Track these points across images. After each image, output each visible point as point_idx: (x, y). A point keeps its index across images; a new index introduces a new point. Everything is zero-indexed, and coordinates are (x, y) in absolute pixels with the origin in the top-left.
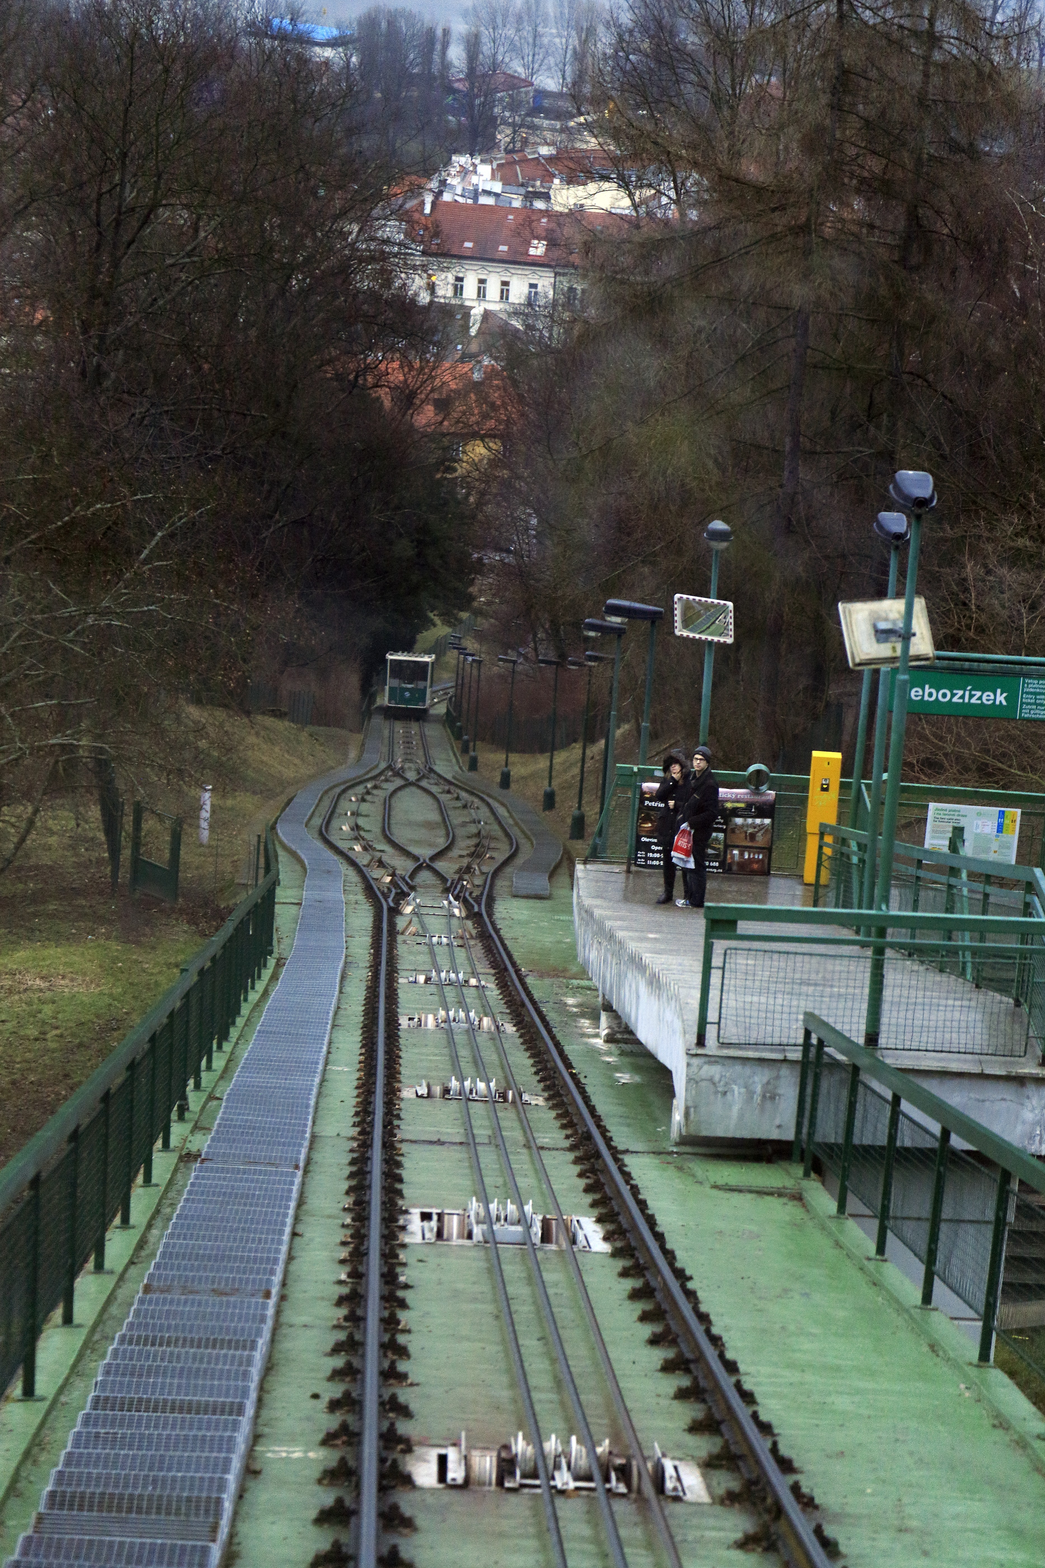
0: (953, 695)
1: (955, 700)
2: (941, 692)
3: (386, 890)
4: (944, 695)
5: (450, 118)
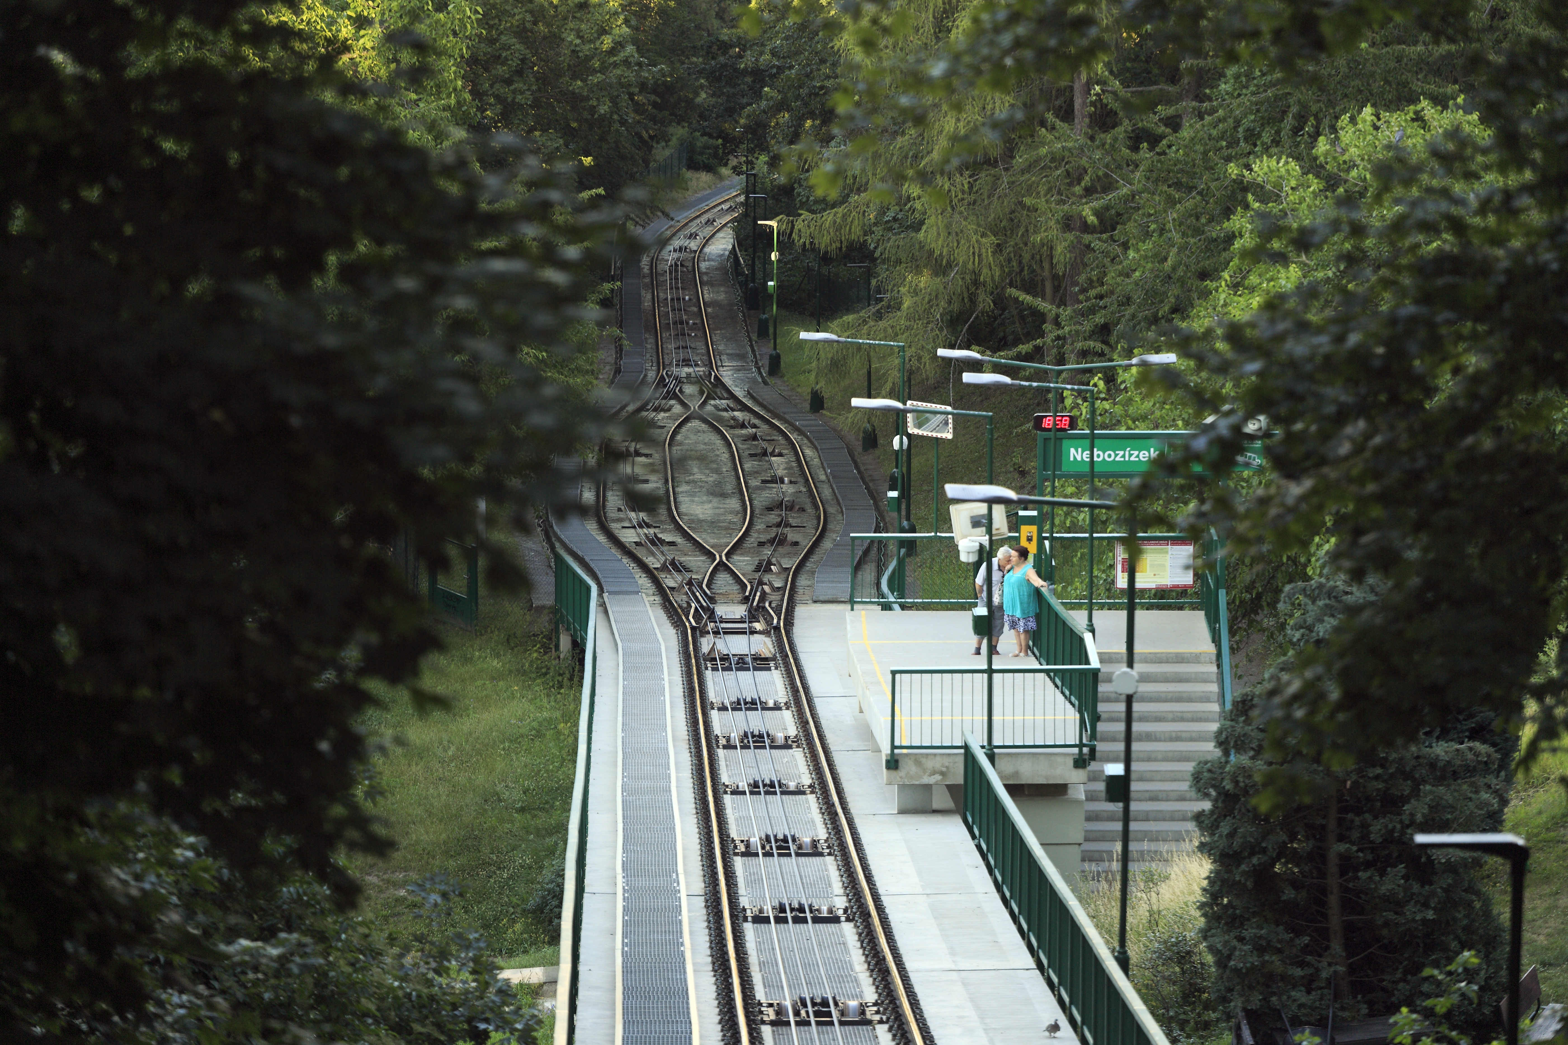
0: (1116, 455)
1: (1118, 459)
2: (1101, 459)
3: (685, 605)
4: (1110, 456)
5: (58, 57)
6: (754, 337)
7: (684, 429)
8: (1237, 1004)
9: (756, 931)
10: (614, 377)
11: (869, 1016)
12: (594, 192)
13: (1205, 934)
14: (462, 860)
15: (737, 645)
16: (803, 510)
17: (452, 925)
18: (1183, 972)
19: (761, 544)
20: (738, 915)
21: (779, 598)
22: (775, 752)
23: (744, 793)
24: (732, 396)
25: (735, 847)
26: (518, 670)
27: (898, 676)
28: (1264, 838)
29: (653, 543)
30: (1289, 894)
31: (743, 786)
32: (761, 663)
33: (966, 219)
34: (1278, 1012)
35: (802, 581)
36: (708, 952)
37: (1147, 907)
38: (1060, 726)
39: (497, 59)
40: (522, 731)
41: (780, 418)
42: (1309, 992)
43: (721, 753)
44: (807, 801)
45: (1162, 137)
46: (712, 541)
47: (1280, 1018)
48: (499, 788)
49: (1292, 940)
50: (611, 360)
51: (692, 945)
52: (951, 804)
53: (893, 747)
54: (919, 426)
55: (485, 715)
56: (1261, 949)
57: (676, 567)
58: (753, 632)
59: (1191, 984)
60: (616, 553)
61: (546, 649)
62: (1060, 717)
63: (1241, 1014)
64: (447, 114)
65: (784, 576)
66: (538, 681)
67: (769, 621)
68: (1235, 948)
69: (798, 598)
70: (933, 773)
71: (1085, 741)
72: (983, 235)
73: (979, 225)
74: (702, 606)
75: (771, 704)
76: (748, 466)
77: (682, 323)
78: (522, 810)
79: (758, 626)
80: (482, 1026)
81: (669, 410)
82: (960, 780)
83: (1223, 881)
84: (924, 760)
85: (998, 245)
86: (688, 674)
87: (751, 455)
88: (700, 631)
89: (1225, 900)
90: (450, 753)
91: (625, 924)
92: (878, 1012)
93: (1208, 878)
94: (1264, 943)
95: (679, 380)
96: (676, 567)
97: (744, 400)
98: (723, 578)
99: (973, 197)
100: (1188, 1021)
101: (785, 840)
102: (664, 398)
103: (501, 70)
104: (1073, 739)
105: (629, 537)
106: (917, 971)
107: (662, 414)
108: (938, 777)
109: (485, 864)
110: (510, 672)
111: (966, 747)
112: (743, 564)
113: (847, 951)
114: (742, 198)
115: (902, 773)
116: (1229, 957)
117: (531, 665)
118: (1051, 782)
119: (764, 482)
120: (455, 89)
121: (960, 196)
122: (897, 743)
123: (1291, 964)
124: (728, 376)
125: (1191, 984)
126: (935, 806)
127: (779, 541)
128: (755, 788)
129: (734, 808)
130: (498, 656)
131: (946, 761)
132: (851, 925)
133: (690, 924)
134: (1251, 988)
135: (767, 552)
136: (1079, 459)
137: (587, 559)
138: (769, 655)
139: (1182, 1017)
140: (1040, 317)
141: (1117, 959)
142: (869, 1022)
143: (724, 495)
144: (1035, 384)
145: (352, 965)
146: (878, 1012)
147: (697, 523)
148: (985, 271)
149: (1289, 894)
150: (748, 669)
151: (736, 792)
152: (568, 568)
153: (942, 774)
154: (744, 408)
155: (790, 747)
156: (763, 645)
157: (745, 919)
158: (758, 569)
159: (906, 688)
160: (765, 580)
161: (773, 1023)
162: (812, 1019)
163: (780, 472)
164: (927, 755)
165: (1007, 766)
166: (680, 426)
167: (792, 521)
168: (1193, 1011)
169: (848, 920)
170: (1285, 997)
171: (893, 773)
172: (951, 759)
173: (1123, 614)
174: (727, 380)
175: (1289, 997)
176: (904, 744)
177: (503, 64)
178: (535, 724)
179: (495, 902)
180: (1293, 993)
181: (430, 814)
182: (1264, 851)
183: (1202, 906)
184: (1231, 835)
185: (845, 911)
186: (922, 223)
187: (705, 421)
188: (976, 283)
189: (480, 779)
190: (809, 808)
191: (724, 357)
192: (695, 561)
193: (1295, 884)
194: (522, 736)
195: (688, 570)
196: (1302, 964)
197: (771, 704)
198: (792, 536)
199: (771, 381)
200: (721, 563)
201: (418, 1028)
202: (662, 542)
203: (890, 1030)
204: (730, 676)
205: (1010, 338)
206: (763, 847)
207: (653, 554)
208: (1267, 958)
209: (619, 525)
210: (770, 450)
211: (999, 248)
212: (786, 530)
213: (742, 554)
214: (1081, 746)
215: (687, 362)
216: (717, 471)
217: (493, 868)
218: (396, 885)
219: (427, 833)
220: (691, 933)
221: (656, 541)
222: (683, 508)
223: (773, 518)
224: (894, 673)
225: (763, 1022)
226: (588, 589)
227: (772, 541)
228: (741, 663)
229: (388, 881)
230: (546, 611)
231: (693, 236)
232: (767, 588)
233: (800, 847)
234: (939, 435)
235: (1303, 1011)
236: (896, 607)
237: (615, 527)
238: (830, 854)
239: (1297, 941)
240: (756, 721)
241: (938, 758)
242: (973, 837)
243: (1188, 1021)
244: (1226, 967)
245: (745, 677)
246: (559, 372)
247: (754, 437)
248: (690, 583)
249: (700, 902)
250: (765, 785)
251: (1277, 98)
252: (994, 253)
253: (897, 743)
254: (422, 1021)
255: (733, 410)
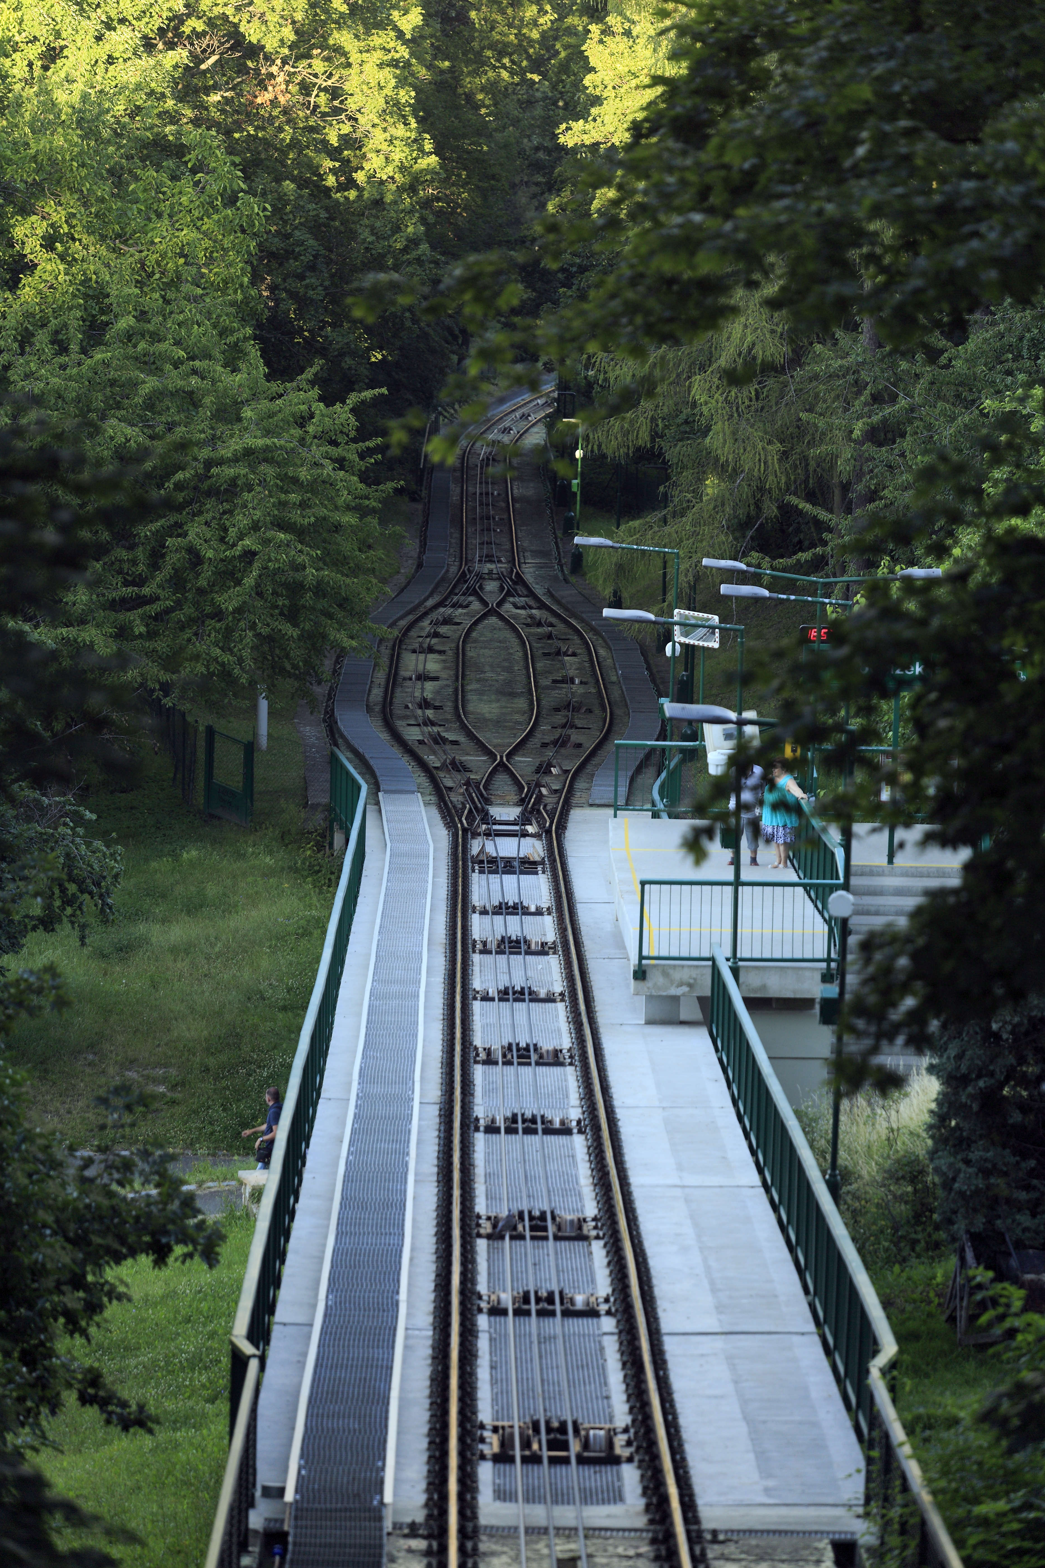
6: (560, 534)
7: (480, 627)
8: (960, 1226)
9: (486, 1141)
10: (417, 571)
11: (585, 1231)
12: (377, 391)
13: (933, 1154)
14: (223, 1058)
15: (507, 848)
16: (590, 711)
17: (210, 1123)
18: (916, 1191)
19: (544, 745)
20: (469, 1124)
21: (555, 800)
22: (529, 958)
23: (493, 999)
24: (531, 594)
25: (477, 1055)
26: (290, 868)
27: (647, 887)
28: (991, 1062)
29: (436, 742)
30: (1016, 1117)
31: (493, 992)
32: (528, 866)
33: (752, 426)
34: (1002, 1235)
35: (580, 784)
36: (435, 1162)
37: (885, 1124)
38: (809, 939)
39: (289, 254)
40: (290, 929)
41: (576, 617)
42: (1034, 1215)
43: (476, 958)
44: (556, 1009)
45: (942, 352)
46: (496, 741)
47: (1004, 1241)
48: (263, 986)
49: (1018, 1163)
50: (415, 554)
51: (418, 1155)
52: (698, 1015)
53: (641, 957)
54: (686, 635)
55: (254, 913)
56: (986, 1173)
57: (457, 767)
58: (525, 834)
59: (923, 1205)
60: (396, 751)
61: (320, 847)
62: (808, 931)
63: (964, 1237)
64: (232, 310)
65: (562, 778)
66: (309, 879)
67: (541, 825)
68: (960, 1171)
69: (574, 800)
70: (681, 984)
71: (833, 955)
72: (770, 442)
73: (766, 433)
74: (476, 808)
75: (533, 909)
76: (539, 665)
77: (488, 518)
78: (284, 1009)
79: (530, 829)
80: (164, 1240)
81: (467, 606)
82: (708, 993)
83: (951, 1104)
84: (671, 972)
85: (784, 452)
86: (454, 877)
87: (545, 654)
88: (470, 833)
89: (953, 1123)
90: (217, 949)
91: (354, 1132)
92: (596, 1228)
93: (936, 1100)
94: (989, 1166)
95: (480, 577)
96: (457, 767)
97: (543, 598)
98: (502, 779)
99: (760, 404)
100: (918, 1241)
101: (527, 1049)
102: (464, 594)
103: (293, 265)
104: (821, 953)
105: (413, 734)
106: (642, 1186)
107: (460, 610)
108: (685, 989)
109: (246, 1062)
110: (283, 869)
111: (713, 959)
112: (524, 764)
113: (575, 1164)
114: (556, 395)
115: (649, 983)
116: (954, 1179)
117: (303, 863)
118: (798, 996)
119: (554, 681)
120: (241, 285)
121: (747, 403)
122: (645, 953)
123: (1017, 1188)
124: (529, 573)
125: (923, 1205)
126: (683, 1017)
127: (561, 743)
128: (504, 995)
129: (482, 1015)
130: (271, 853)
131: (694, 973)
132: (583, 1137)
133: (419, 1133)
134: (975, 1210)
135: (549, 753)
137: (367, 756)
138: (537, 859)
139: (913, 1236)
140: (820, 526)
141: (828, 1182)
142: (585, 1238)
143: (512, 695)
144: (793, 597)
145: (30, 1176)
146: (596, 1228)
147: (483, 722)
148: (770, 478)
149: (1016, 1117)
150: (514, 873)
151: (486, 998)
152: (342, 766)
153: (690, 985)
154: (542, 606)
155: (547, 954)
156: (533, 848)
157: (477, 1129)
158: (537, 771)
159: (655, 897)
160: (543, 782)
161: (489, 1237)
162: (528, 1234)
163: (572, 672)
164: (675, 966)
165: (754, 980)
166: (476, 623)
167: (578, 723)
168: (924, 1230)
169: (580, 1132)
170: (1009, 1221)
171: (641, 984)
172: (699, 971)
174: (529, 578)
175: (1014, 1221)
176: (652, 954)
177: (296, 259)
178: (303, 922)
179: (254, 1101)
180: (1018, 1217)
181: (192, 1010)
182: (992, 1074)
183: (930, 1127)
184: (959, 1057)
185: (579, 1122)
186: (708, 429)
187: (501, 617)
188: (761, 489)
189: (247, 975)
190: (557, 1016)
191: (528, 554)
192: (476, 761)
193: (1023, 1107)
194: (289, 934)
195: (466, 769)
196: (1028, 1188)
197: (533, 909)
198: (575, 737)
199: (573, 579)
200: (501, 764)
201: (97, 1240)
202: (445, 740)
203: (605, 1246)
204: (494, 879)
205: (806, 543)
206: (504, 1056)
207: (434, 753)
208: (992, 1181)
209: (404, 723)
210: (564, 649)
211: (784, 455)
212: (570, 732)
213: (524, 755)
214: (829, 960)
215: (490, 558)
216: (509, 670)
217: (253, 1067)
218: (156, 1081)
219: (189, 1029)
220: (419, 1142)
221: (438, 740)
222: (471, 707)
223: (559, 719)
224: (643, 883)
225: (479, 1236)
226: (359, 788)
227: (555, 743)
228: (508, 866)
229: (148, 1077)
230: (320, 809)
231: (506, 430)
232: (544, 791)
233: (541, 1057)
234: (706, 644)
235: (1027, 1235)
236: (664, 815)
237: (400, 725)
238: (571, 1064)
239: (1023, 1165)
240: (513, 926)
241: (686, 970)
242: (717, 1050)
243: (918, 1241)
244: (951, 1189)
245: (510, 880)
246: (338, 572)
247: (550, 636)
248: (468, 783)
249: (434, 1112)
250: (514, 993)
252: (780, 460)
253: (645, 953)
254: (103, 1234)
255: (531, 608)
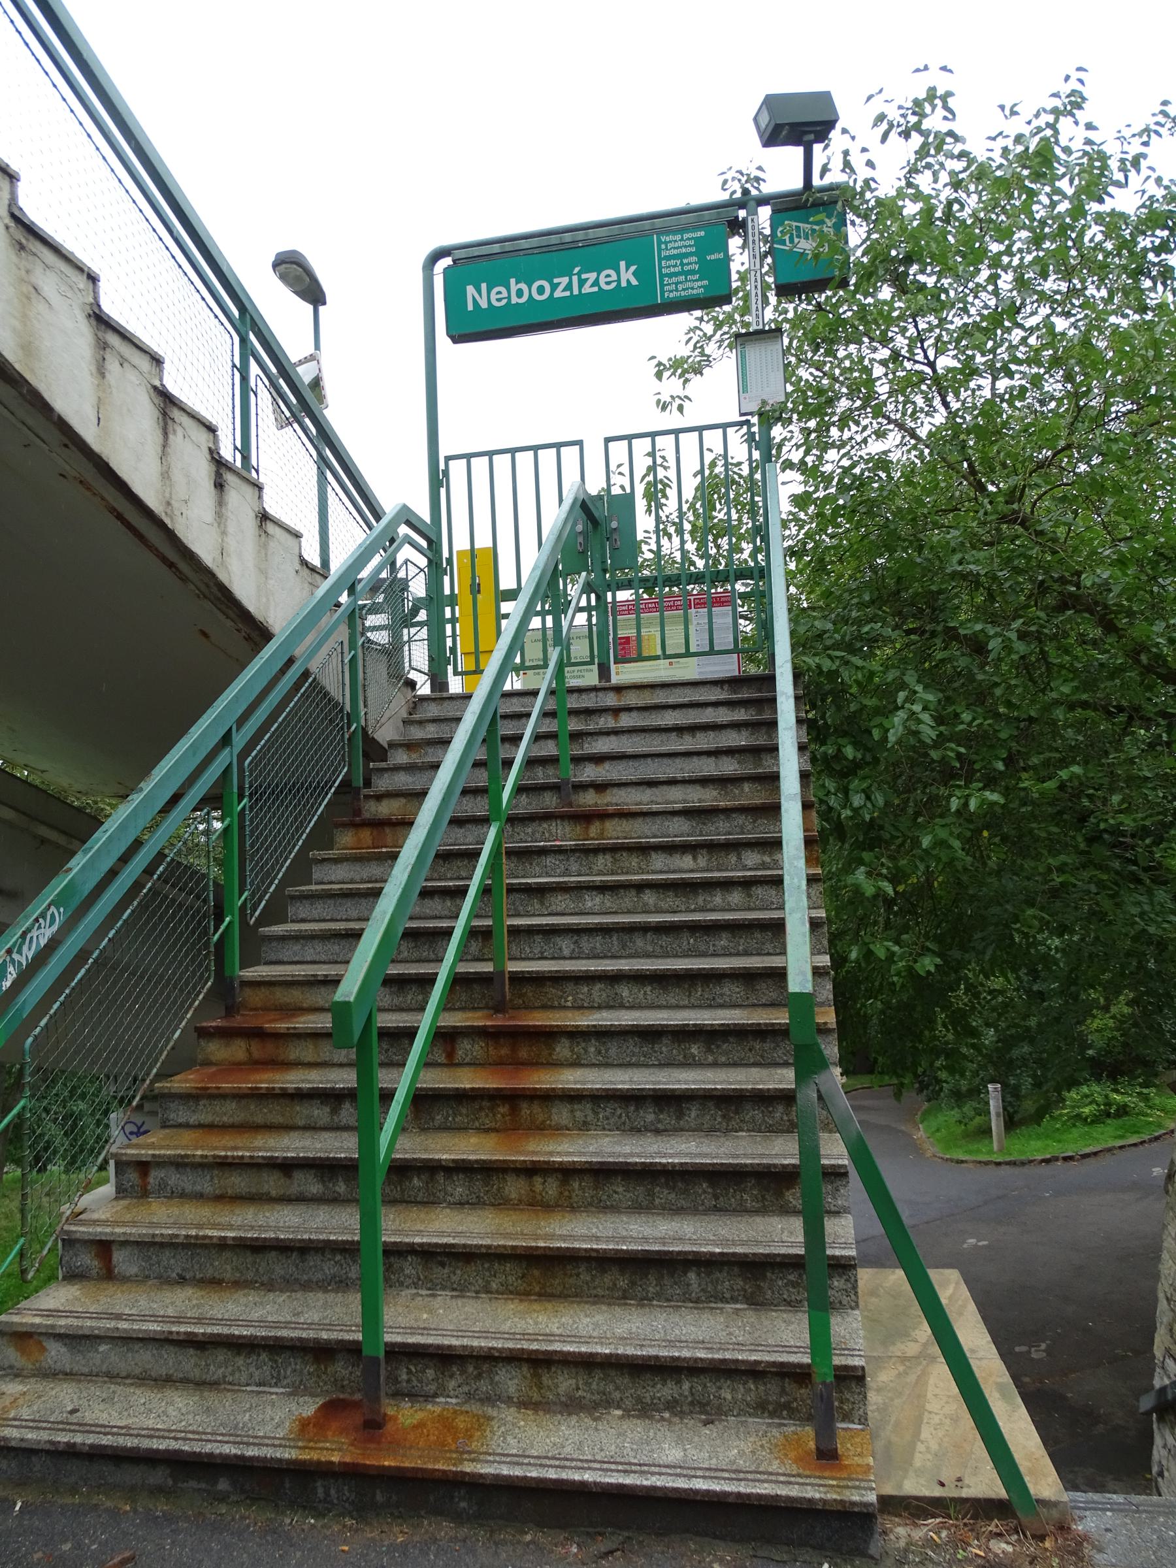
0: (554, 287)
136: (484, 304)
173: (477, 546)
224: (580, 443)
251: (319, 1441)
